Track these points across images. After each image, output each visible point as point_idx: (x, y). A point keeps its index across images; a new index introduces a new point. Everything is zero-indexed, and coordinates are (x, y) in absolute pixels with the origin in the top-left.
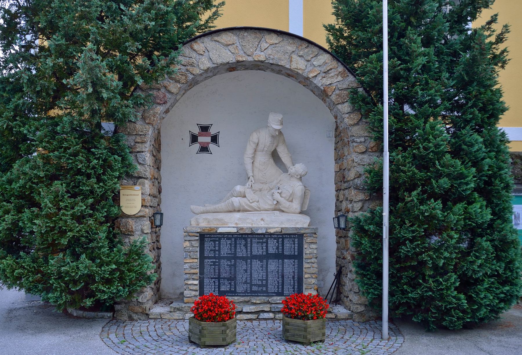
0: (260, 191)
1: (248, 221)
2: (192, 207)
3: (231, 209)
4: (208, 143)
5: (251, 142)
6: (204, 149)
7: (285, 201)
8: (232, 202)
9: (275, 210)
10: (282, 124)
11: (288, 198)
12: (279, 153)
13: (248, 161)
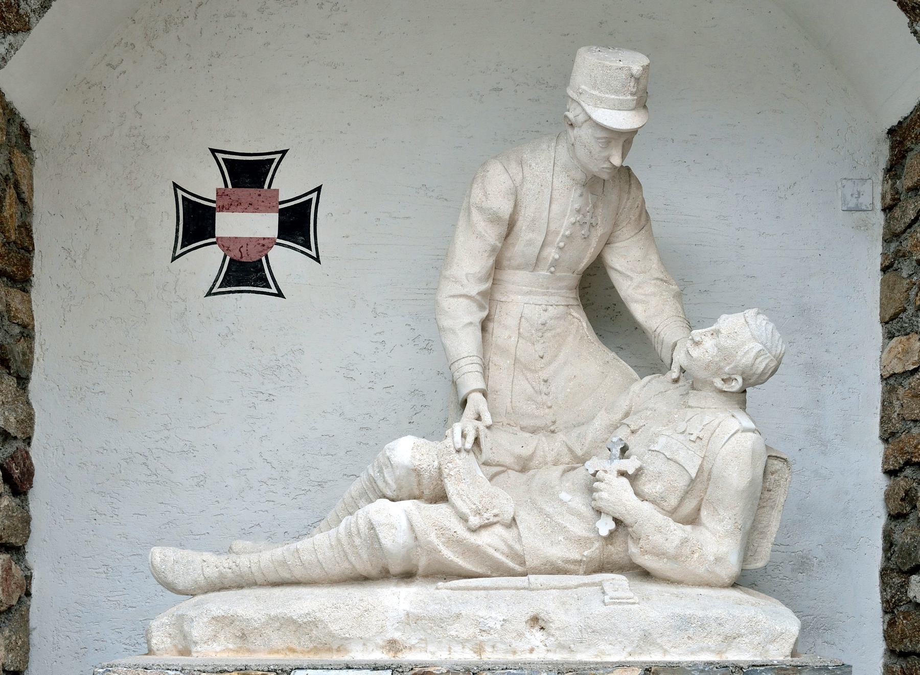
0: (524, 469)
1: (455, 629)
2: (158, 554)
3: (363, 565)
4: (265, 245)
5: (476, 216)
6: (245, 273)
7: (660, 518)
8: (372, 527)
9: (602, 568)
10: (642, 104)
11: (673, 501)
12: (615, 277)
13: (460, 316)
